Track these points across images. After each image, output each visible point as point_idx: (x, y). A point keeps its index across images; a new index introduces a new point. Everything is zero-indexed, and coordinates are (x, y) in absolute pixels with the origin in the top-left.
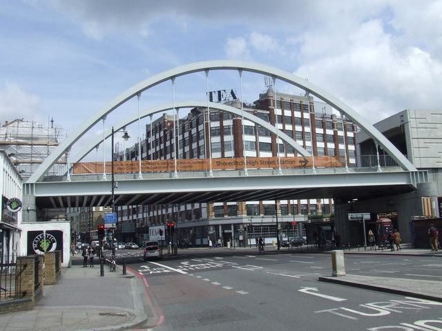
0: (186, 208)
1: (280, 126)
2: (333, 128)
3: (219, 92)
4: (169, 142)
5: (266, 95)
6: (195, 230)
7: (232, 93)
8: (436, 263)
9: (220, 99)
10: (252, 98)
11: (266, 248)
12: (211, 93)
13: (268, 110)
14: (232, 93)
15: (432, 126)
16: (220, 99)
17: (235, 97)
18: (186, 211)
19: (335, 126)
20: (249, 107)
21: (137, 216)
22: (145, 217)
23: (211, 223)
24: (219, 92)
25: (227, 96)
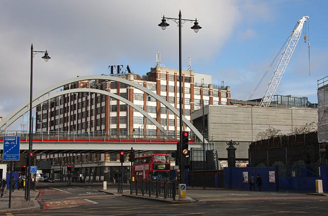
0: (70, 155)
1: (115, 91)
2: (209, 95)
3: (118, 66)
4: (80, 109)
5: (155, 69)
6: (96, 170)
7: (128, 68)
8: (297, 199)
9: (118, 72)
10: (144, 72)
11: (47, 209)
12: (112, 67)
13: (156, 81)
14: (128, 68)
15: (224, 116)
16: (118, 72)
17: (129, 72)
18: (41, 160)
19: (211, 94)
20: (311, 106)
21: (54, 156)
22: (60, 157)
23: (107, 164)
24: (118, 66)
25: (124, 70)
